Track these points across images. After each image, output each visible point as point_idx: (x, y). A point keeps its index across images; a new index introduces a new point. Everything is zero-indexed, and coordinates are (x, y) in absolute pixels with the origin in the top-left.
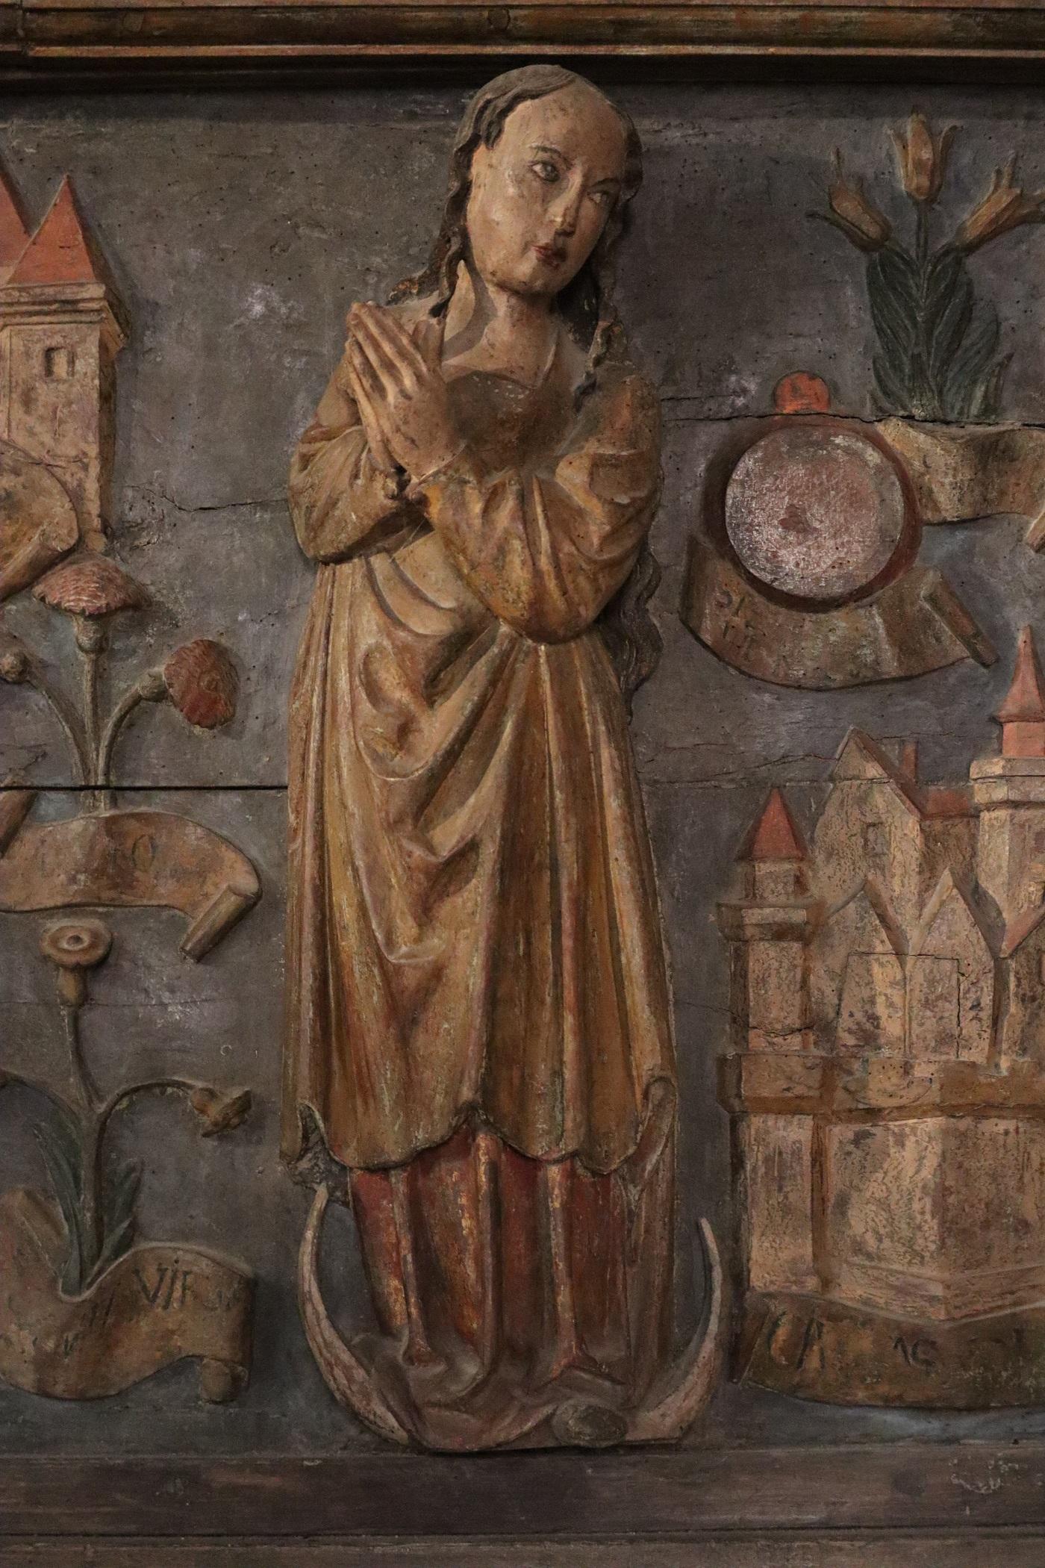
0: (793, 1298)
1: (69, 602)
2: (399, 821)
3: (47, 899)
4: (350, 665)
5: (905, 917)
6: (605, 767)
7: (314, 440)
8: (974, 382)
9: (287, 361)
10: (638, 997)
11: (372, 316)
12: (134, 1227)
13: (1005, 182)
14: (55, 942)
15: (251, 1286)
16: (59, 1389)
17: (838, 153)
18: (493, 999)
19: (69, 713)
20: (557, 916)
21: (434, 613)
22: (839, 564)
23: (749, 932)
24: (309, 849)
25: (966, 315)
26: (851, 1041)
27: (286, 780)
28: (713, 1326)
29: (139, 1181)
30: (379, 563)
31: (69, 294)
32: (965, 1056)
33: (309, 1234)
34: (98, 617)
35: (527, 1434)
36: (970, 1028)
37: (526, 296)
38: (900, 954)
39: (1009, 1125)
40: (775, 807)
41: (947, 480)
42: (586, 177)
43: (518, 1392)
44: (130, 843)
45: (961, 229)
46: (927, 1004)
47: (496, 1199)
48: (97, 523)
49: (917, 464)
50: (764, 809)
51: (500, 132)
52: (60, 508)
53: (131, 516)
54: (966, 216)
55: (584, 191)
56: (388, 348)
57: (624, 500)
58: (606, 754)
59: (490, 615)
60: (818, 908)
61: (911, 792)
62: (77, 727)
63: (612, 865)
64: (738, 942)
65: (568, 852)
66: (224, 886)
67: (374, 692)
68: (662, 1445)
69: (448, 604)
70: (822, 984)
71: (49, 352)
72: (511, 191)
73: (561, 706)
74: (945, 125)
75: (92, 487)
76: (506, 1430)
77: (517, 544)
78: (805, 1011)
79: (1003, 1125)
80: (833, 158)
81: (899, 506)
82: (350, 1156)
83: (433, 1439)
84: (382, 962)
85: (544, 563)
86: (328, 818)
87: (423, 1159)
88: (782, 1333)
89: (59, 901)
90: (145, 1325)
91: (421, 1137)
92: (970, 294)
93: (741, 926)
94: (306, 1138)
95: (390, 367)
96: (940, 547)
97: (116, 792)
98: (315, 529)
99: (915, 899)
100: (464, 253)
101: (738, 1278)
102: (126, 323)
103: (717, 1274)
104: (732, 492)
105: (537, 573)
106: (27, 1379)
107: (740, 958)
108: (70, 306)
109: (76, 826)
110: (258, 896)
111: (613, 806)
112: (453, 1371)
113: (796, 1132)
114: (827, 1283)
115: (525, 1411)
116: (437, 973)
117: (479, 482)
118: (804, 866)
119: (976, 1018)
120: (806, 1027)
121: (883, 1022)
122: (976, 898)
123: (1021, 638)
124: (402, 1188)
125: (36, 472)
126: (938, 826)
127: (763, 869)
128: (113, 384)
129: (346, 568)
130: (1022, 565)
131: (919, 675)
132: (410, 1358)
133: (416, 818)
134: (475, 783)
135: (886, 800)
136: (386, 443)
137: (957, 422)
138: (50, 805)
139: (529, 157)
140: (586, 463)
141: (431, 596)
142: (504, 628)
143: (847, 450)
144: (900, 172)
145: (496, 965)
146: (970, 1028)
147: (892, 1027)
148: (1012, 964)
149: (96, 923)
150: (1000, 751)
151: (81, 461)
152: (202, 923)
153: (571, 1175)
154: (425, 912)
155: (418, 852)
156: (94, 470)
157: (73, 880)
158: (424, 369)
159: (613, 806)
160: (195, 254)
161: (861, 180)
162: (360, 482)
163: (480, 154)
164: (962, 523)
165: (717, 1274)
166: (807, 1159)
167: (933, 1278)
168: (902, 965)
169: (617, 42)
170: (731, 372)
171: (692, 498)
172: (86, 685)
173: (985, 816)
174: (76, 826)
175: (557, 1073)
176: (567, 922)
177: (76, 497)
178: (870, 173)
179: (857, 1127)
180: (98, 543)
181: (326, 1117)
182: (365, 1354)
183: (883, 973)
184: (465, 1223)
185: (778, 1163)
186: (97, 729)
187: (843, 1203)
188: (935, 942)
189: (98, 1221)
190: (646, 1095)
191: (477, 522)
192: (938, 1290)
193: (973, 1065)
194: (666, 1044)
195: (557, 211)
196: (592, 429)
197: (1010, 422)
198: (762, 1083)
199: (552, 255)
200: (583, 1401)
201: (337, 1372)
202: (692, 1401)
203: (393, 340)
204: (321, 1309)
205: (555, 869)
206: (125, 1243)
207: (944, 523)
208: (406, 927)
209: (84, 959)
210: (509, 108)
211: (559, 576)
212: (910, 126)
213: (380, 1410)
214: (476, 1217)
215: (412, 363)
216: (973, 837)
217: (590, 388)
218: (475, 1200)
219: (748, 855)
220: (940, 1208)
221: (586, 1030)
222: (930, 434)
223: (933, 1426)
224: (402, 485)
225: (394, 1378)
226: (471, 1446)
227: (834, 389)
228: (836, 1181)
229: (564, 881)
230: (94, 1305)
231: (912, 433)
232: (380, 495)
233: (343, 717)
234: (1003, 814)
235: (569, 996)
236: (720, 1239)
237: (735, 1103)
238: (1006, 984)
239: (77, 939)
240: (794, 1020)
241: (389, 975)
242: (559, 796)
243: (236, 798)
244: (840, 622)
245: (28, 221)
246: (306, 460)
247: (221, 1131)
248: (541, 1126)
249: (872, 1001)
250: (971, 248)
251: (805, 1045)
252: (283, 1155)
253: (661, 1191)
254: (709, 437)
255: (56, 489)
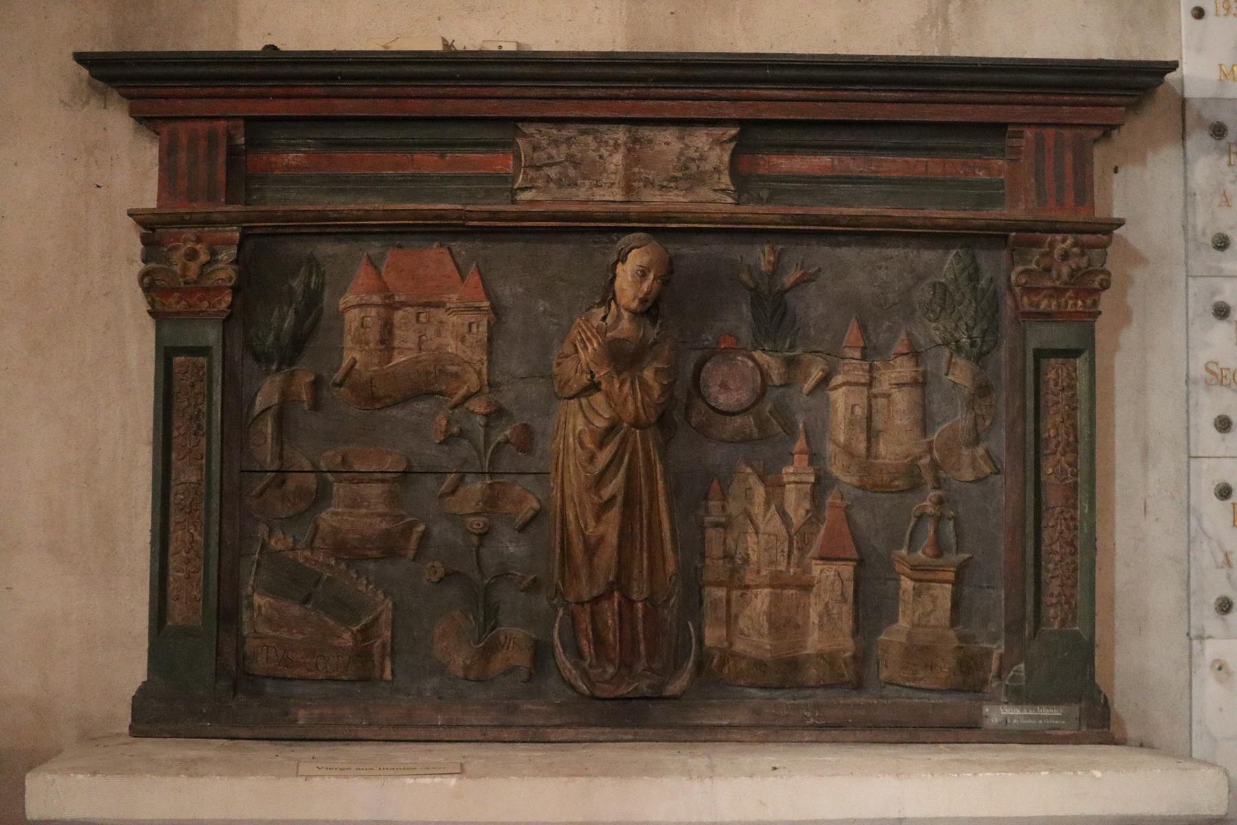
0: (720, 649)
1: (477, 410)
2: (590, 488)
3: (469, 511)
4: (574, 436)
5: (759, 521)
6: (658, 471)
7: (562, 358)
8: (786, 338)
9: (551, 327)
10: (668, 546)
11: (584, 323)
12: (496, 622)
13: (799, 267)
14: (471, 525)
15: (536, 641)
16: (471, 677)
17: (741, 257)
18: (620, 547)
19: (476, 448)
20: (642, 520)
21: (601, 419)
22: (738, 400)
23: (706, 524)
24: (559, 496)
25: (784, 314)
26: (739, 562)
27: (549, 471)
28: (692, 658)
29: (498, 607)
30: (584, 401)
31: (477, 304)
32: (779, 568)
33: (557, 625)
34: (486, 415)
35: (630, 692)
36: (780, 558)
37: (635, 314)
38: (757, 533)
39: (793, 591)
40: (715, 483)
41: (776, 372)
42: (655, 275)
43: (627, 678)
44: (496, 492)
45: (782, 286)
46: (766, 550)
47: (620, 614)
48: (486, 383)
49: (766, 366)
50: (712, 482)
51: (626, 259)
52: (474, 377)
53: (497, 380)
54: (785, 279)
55: (654, 279)
56: (589, 334)
57: (665, 383)
58: (659, 466)
59: (621, 420)
60: (730, 516)
61: (762, 478)
62: (478, 452)
63: (660, 503)
64: (702, 528)
65: (645, 498)
66: (528, 507)
67: (581, 443)
68: (674, 698)
69: (607, 416)
70: (730, 542)
71: (470, 324)
72: (630, 278)
73: (644, 449)
74: (780, 247)
75: (485, 371)
76: (623, 691)
77: (630, 398)
78: (725, 551)
79: (792, 592)
80: (739, 259)
81: (759, 381)
82: (571, 599)
83: (598, 693)
84: (583, 534)
85: (639, 404)
86: (565, 485)
87: (596, 600)
88: (715, 661)
89: (473, 511)
90: (500, 656)
91: (595, 593)
92: (786, 307)
93: (703, 523)
94: (556, 592)
95: (589, 339)
96: (775, 394)
97: (491, 474)
98: (562, 388)
99: (762, 514)
100: (614, 298)
101: (701, 641)
102: (496, 314)
103: (694, 640)
104: (703, 374)
105: (637, 408)
106: (460, 674)
107: (703, 533)
108: (478, 309)
109: (479, 486)
110: (540, 511)
111: (661, 484)
112: (605, 672)
113: (721, 593)
114: (731, 644)
115: (629, 684)
116: (601, 539)
117: (618, 377)
118: (726, 503)
119: (783, 555)
120: (725, 557)
121: (751, 556)
122: (783, 514)
123: (801, 425)
124: (588, 610)
125: (466, 365)
126: (770, 489)
127: (711, 503)
128: (492, 335)
129: (572, 401)
130: (801, 400)
131: (290, 679)
132: (590, 666)
133: (595, 487)
134: (615, 476)
135: (753, 481)
136: (588, 364)
137: (781, 351)
138: (468, 479)
139: (636, 268)
140: (654, 370)
141: (601, 413)
142: (625, 425)
143: (742, 361)
144: (763, 264)
145: (622, 536)
146: (780, 558)
147: (754, 558)
148: (795, 537)
149: (484, 519)
150: (792, 464)
151: (481, 361)
152: (520, 520)
153: (645, 606)
154: (598, 519)
155: (596, 498)
156: (486, 364)
157: (478, 504)
158: (601, 340)
159: (661, 484)
160: (520, 290)
161: (749, 266)
162: (578, 374)
163: (620, 265)
164: (781, 386)
165: (694, 640)
166: (724, 603)
167: (767, 643)
168: (758, 537)
169: (665, 223)
170: (703, 333)
171: (689, 376)
172: (482, 438)
173: (787, 486)
174: (479, 486)
175: (641, 572)
176: (645, 522)
177: (479, 373)
178: (752, 264)
179: (742, 591)
180: (486, 390)
181: (563, 586)
182: (576, 666)
183: (751, 539)
184: (610, 622)
185: (715, 604)
186: (485, 453)
187: (737, 616)
188: (770, 529)
189: (485, 620)
190: (670, 579)
191: (617, 390)
192: (768, 647)
193: (781, 571)
194: (677, 562)
195: (645, 287)
196: (654, 359)
197: (798, 352)
198: (709, 576)
199: (643, 301)
200: (648, 682)
201: (566, 671)
202: (685, 683)
203: (591, 332)
204: (561, 650)
205: (641, 504)
206: (494, 628)
207: (775, 386)
208: (592, 523)
209: (482, 531)
210: (630, 251)
211: (644, 409)
212: (767, 248)
213: (581, 684)
214: (613, 620)
215: (596, 338)
216: (783, 494)
217: (655, 343)
218: (613, 614)
219: (706, 498)
220: (769, 620)
221: (650, 558)
222: (770, 355)
223: (766, 694)
224: (593, 376)
225: (585, 674)
226: (612, 696)
227: (738, 339)
228: (734, 611)
229: (644, 508)
230: (484, 648)
231: (765, 355)
232: (586, 379)
233: (571, 451)
234: (793, 486)
235: (645, 546)
236: (695, 629)
237: (701, 583)
238: (793, 544)
239: (479, 525)
240: (721, 554)
241: (586, 540)
242: (643, 480)
243: (533, 477)
244: (738, 420)
245: (463, 278)
246: (559, 364)
247: (525, 590)
248: (636, 589)
249: (747, 549)
250: (786, 291)
251: (724, 562)
252: (547, 598)
253: (675, 612)
254: (695, 356)
255: (472, 370)
